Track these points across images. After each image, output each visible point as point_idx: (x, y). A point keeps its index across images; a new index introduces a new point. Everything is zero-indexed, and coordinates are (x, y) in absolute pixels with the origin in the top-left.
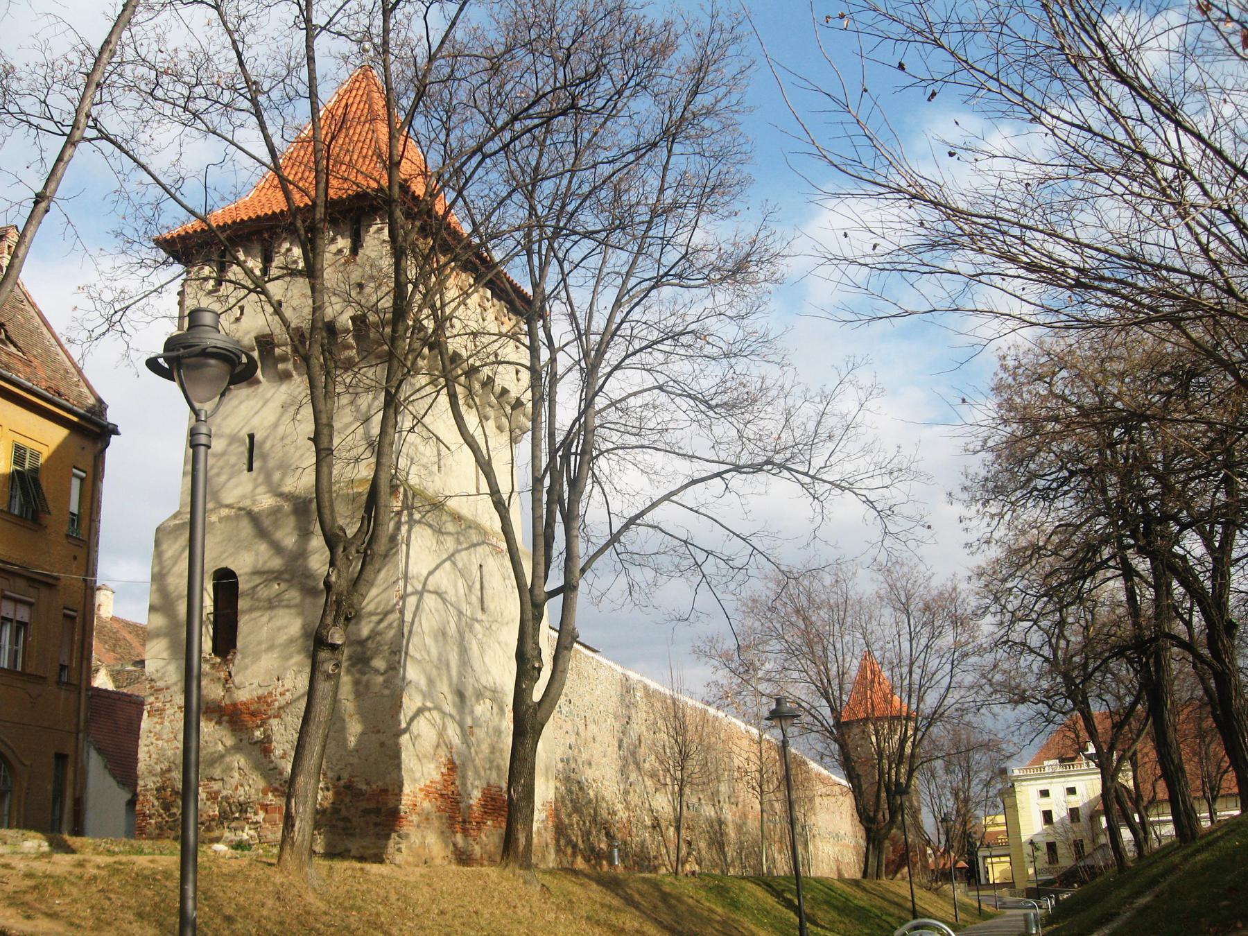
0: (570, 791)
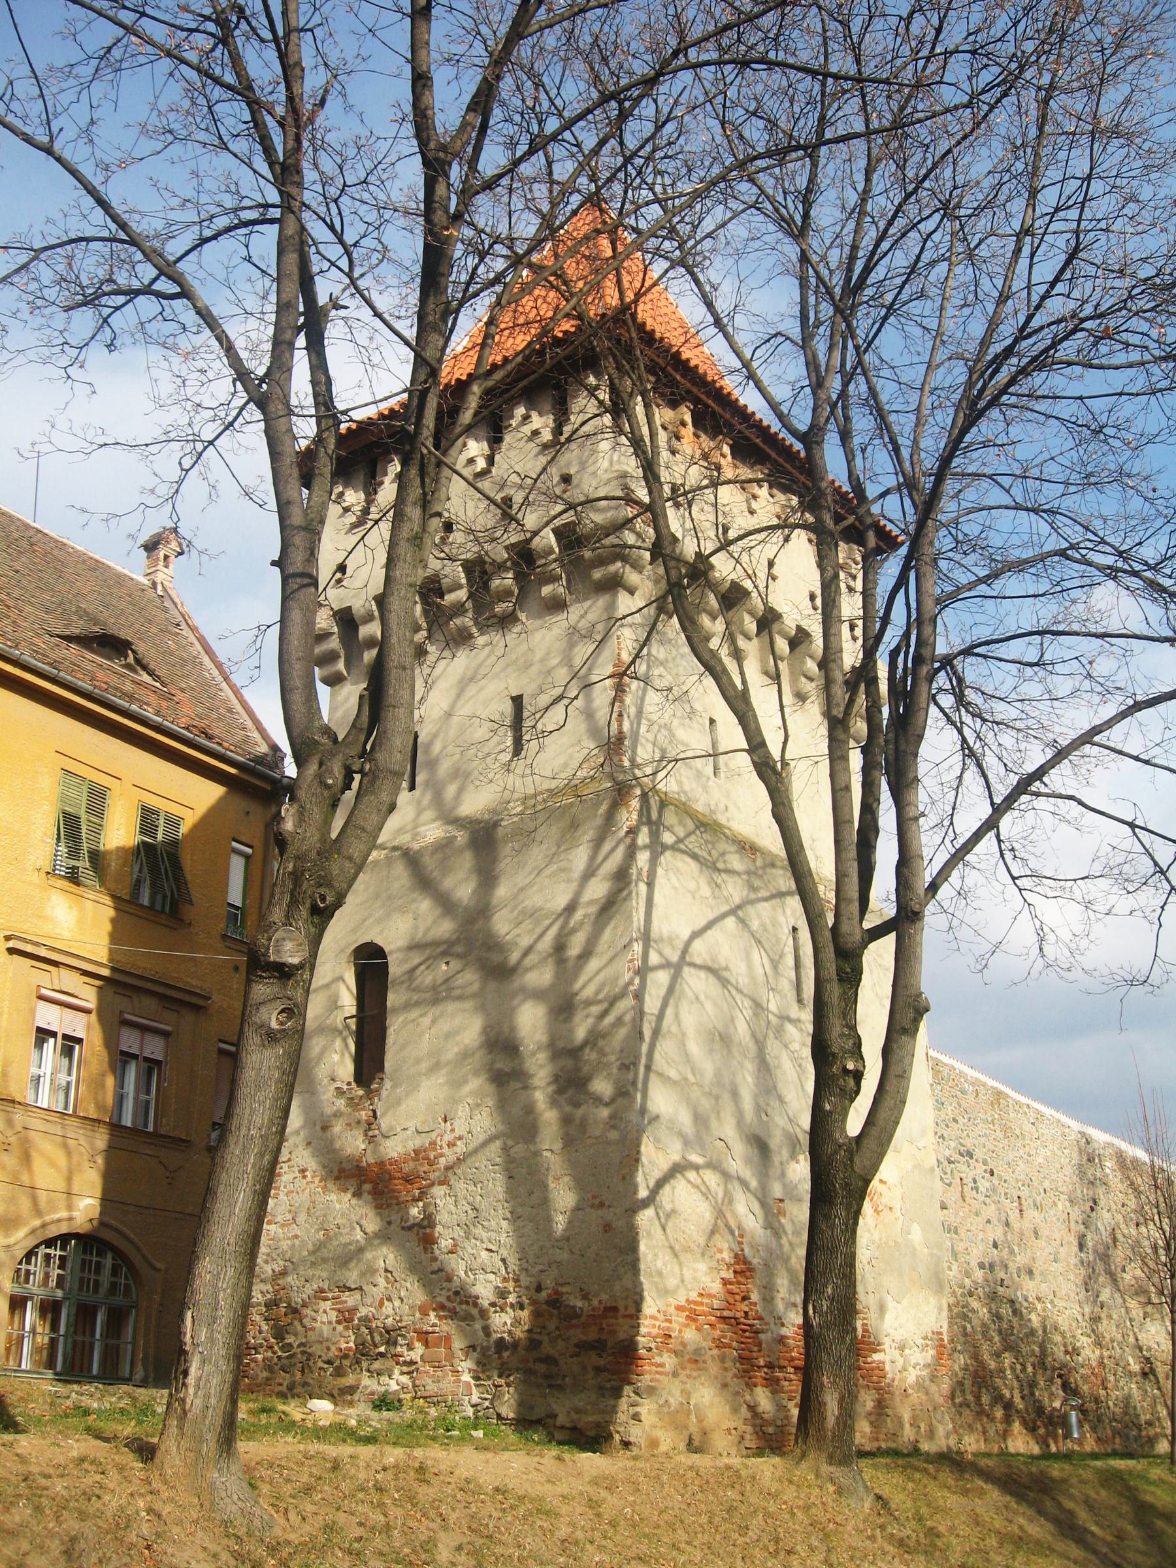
0: (998, 1317)
